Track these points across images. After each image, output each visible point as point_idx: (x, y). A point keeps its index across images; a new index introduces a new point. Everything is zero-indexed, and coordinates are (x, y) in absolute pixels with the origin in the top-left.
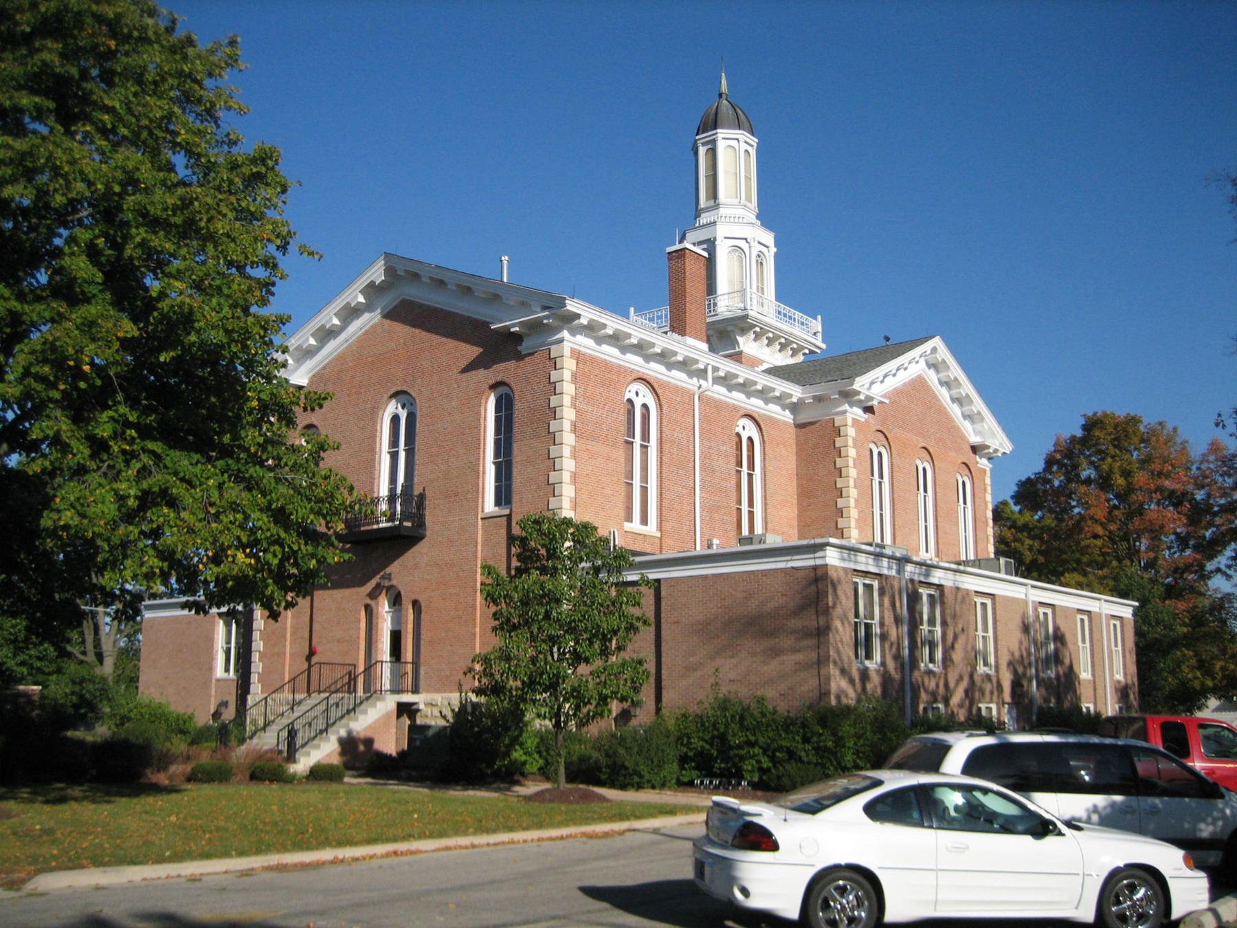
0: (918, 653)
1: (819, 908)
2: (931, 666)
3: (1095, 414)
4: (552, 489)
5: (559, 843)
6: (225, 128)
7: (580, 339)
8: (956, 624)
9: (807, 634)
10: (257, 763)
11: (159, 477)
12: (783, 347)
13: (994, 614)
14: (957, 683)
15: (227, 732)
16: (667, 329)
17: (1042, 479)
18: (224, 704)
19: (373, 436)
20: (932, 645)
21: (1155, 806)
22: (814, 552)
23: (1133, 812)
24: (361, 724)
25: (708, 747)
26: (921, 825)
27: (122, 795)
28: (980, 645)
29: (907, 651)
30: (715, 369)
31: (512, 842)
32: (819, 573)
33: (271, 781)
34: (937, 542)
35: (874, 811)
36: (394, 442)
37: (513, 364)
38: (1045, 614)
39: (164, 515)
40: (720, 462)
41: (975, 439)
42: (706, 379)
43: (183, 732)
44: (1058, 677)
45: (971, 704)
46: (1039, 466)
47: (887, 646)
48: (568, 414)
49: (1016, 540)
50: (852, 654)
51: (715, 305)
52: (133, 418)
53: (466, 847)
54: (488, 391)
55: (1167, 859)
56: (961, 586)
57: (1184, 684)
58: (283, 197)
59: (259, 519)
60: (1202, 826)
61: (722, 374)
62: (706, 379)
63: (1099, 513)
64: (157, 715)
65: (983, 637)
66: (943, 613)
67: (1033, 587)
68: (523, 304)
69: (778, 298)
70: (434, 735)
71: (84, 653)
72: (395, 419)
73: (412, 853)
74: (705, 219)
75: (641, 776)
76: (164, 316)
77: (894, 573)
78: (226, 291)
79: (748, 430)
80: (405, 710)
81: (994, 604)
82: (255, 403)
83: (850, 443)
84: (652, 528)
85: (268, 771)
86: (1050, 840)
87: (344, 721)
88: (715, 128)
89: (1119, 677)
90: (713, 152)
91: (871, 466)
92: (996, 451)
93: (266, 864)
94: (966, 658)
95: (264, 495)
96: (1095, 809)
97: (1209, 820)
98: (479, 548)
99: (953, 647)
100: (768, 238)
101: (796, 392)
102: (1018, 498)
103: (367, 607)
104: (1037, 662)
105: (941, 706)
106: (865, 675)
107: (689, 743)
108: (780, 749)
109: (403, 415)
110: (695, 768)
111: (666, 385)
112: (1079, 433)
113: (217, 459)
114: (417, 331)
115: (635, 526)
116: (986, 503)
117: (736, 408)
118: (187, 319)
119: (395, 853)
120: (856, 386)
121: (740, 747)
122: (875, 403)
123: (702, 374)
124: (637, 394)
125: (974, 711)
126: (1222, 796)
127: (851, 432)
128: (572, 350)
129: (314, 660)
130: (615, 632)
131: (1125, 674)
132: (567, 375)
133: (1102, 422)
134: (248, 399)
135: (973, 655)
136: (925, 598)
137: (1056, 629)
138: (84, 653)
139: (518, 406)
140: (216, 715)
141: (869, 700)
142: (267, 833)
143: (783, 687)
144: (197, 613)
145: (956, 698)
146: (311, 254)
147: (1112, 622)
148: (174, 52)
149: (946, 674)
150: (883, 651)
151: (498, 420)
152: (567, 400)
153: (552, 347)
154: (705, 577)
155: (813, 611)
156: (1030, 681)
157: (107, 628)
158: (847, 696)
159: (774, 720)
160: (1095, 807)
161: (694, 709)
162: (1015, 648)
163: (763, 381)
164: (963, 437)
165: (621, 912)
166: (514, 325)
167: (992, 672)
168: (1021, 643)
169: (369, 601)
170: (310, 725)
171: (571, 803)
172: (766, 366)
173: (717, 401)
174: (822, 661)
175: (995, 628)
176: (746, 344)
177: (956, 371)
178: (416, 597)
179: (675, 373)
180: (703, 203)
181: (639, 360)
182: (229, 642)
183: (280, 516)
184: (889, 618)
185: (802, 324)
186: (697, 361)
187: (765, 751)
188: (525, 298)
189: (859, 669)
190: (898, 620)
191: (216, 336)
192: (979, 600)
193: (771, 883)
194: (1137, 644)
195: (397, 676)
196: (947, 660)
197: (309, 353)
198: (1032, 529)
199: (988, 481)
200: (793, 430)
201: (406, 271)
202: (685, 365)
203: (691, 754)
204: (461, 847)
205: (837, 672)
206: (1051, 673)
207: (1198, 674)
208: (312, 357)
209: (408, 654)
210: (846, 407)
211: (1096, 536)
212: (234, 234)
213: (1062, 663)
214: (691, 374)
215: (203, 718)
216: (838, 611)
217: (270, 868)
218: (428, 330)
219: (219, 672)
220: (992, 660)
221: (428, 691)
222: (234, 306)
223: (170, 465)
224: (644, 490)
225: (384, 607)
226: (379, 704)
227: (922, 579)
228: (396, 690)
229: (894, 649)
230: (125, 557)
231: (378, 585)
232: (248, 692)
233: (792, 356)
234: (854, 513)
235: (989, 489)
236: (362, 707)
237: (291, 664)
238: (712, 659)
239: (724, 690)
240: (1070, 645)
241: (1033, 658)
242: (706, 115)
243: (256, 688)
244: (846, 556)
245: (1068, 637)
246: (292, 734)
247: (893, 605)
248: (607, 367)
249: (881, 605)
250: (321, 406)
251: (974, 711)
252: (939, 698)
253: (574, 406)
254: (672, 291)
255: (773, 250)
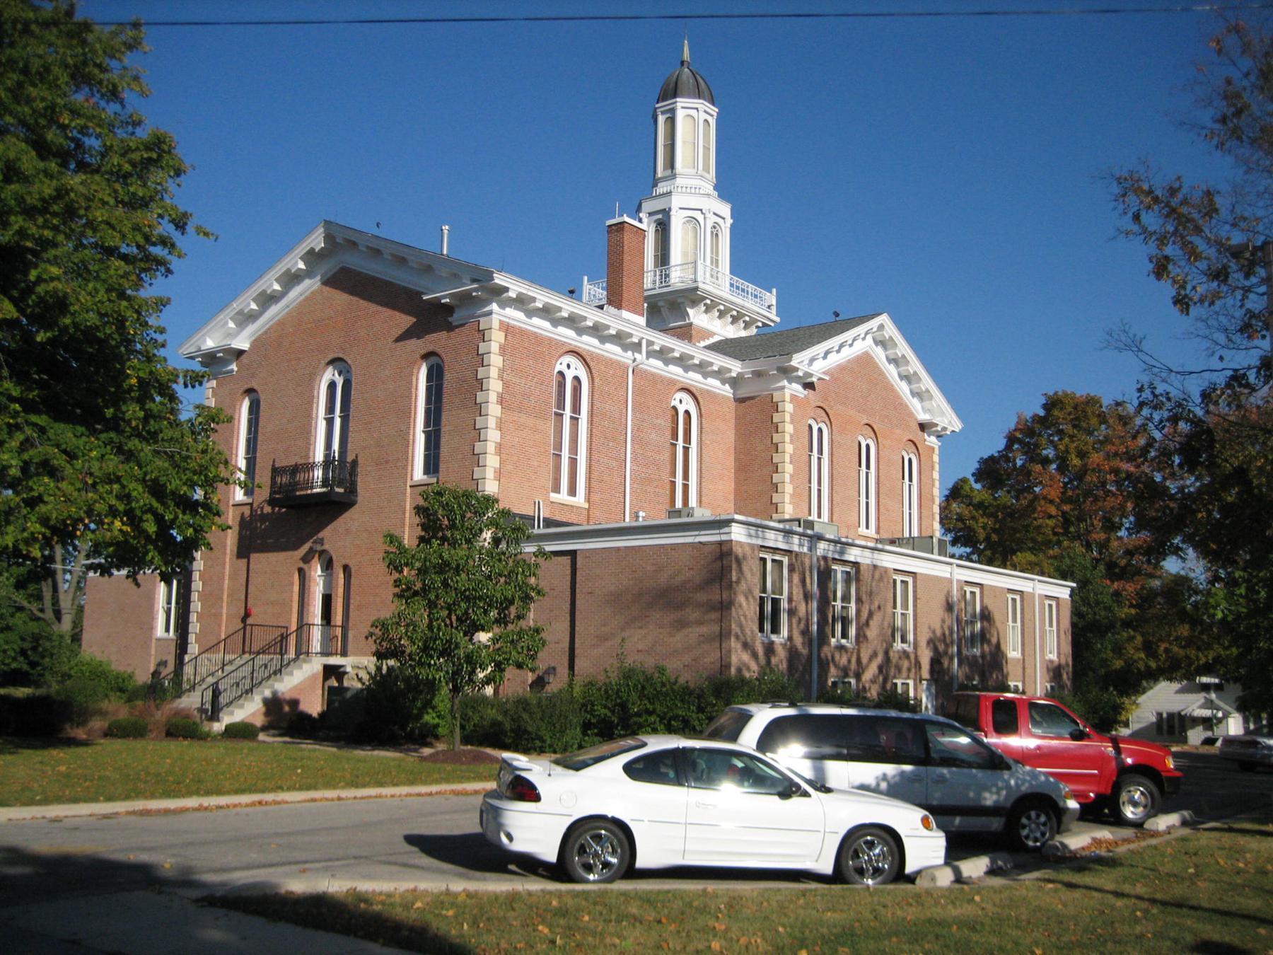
0: (828, 630)
1: (575, 851)
2: (844, 641)
3: (1056, 393)
4: (476, 459)
5: (428, 799)
6: (129, 110)
7: (510, 312)
8: (871, 602)
9: (712, 607)
10: (174, 720)
11: (40, 449)
12: (735, 320)
13: (915, 592)
14: (870, 660)
15: (155, 690)
16: (604, 302)
17: (1005, 456)
18: (163, 663)
19: (310, 400)
20: (845, 622)
21: (942, 776)
22: (720, 528)
23: (920, 780)
24: (287, 685)
25: (609, 714)
26: (680, 784)
27: (28, 747)
28: (899, 623)
29: (815, 627)
30: (650, 343)
31: (380, 796)
32: (725, 548)
33: (185, 737)
34: (878, 519)
35: (632, 770)
36: (330, 409)
37: (444, 334)
38: (973, 593)
39: (46, 485)
40: (653, 435)
41: (923, 417)
42: (640, 352)
43: (122, 690)
44: (983, 656)
45: (885, 680)
46: (1001, 444)
47: (794, 621)
48: (495, 386)
49: (973, 518)
50: (756, 628)
51: (667, 276)
52: (16, 392)
53: (333, 800)
54: (420, 361)
55: (906, 819)
56: (879, 563)
57: (1130, 663)
58: (178, 180)
59: (136, 489)
60: (987, 795)
61: (657, 348)
62: (640, 352)
63: (1053, 493)
64: (98, 672)
65: (905, 615)
66: (858, 590)
67: (958, 566)
68: (455, 276)
69: (732, 272)
70: (352, 697)
71: (42, 610)
72: (332, 386)
73: (276, 803)
74: (662, 188)
75: (544, 741)
76: (41, 300)
77: (805, 550)
78: (103, 276)
79: (685, 403)
80: (329, 671)
81: (915, 582)
82: (134, 381)
83: (788, 418)
84: (580, 499)
85: (183, 729)
86: (796, 801)
87: (270, 682)
88: (675, 95)
89: (1053, 657)
90: (672, 121)
91: (809, 440)
92: (944, 429)
93: (131, 809)
94: (881, 634)
95: (140, 467)
96: (884, 777)
97: (994, 789)
98: (407, 515)
99: (867, 624)
100: (725, 209)
101: (735, 367)
102: (979, 476)
103: (301, 571)
104: (960, 640)
105: (853, 681)
106: (770, 649)
107: (593, 710)
108: (676, 717)
109: (340, 381)
110: (596, 735)
111: (599, 358)
112: (1042, 413)
113: (101, 432)
114: (355, 299)
115: (563, 496)
116: (933, 480)
117: (672, 382)
118: (62, 304)
119: (260, 803)
120: (794, 363)
121: (638, 714)
122: (814, 379)
123: (637, 347)
124: (569, 366)
125: (888, 686)
126: (1008, 768)
127: (789, 407)
128: (501, 322)
129: (250, 621)
130: (511, 602)
131: (1059, 654)
132: (495, 347)
133: (1061, 402)
134: (128, 376)
135: (890, 632)
136: (839, 576)
137: (984, 609)
138: (42, 610)
139: (448, 376)
140: (156, 674)
141: (772, 671)
142: (146, 782)
143: (687, 659)
144: (102, 575)
145: (870, 672)
146: (206, 234)
147: (1047, 602)
148: (72, 38)
149: (859, 651)
150: (790, 626)
151: (429, 389)
152: (494, 372)
153: (481, 319)
154: (618, 549)
155: (717, 586)
156: (951, 659)
157: (66, 586)
158: (748, 669)
159: (673, 691)
160: (885, 775)
161: (601, 678)
162: (937, 626)
163: (699, 355)
164: (911, 415)
165: (423, 855)
166: (444, 297)
167: (909, 649)
168: (943, 621)
169: (302, 565)
170: (238, 685)
171: (463, 763)
172: (716, 339)
173: (653, 375)
174: (723, 635)
175: (915, 606)
176: (697, 317)
177: (903, 348)
178: (347, 562)
179: (608, 346)
180: (660, 173)
181: (571, 333)
182: (169, 602)
183: (157, 490)
184: (798, 594)
185: (756, 296)
186: (631, 335)
187: (662, 719)
188: (456, 270)
189: (763, 643)
190: (807, 597)
191: (92, 318)
192: (899, 578)
193: (534, 830)
194: (1073, 625)
195: (327, 640)
196: (861, 637)
197: (252, 317)
198: (987, 508)
199: (936, 458)
200: (733, 404)
201: (345, 239)
202: (619, 338)
203: (593, 721)
204: (327, 799)
205: (739, 646)
206: (977, 651)
207: (1142, 655)
208: (254, 322)
209: (338, 618)
210: (785, 383)
211: (1050, 517)
212: (113, 221)
213: (989, 642)
214: (625, 347)
215: (143, 677)
216: (743, 586)
217: (134, 813)
218: (364, 299)
219: (160, 631)
220: (911, 637)
221: (355, 654)
222: (109, 290)
223: (52, 437)
224: (573, 462)
225: (316, 572)
226: (306, 667)
227: (837, 556)
228: (325, 653)
229: (802, 625)
230: (8, 523)
231: (311, 549)
232: (186, 653)
233: (745, 328)
234: (789, 489)
235: (937, 467)
236: (289, 669)
237: (227, 623)
238: (623, 629)
239: (629, 661)
240: (998, 624)
241: (955, 636)
242: (666, 84)
243: (193, 648)
244: (753, 532)
245: (997, 616)
246: (216, 694)
247: (803, 581)
248: (537, 339)
249: (790, 581)
250: (201, 384)
251: (888, 686)
252: (851, 674)
253: (501, 378)
254: (610, 265)
255: (729, 221)
